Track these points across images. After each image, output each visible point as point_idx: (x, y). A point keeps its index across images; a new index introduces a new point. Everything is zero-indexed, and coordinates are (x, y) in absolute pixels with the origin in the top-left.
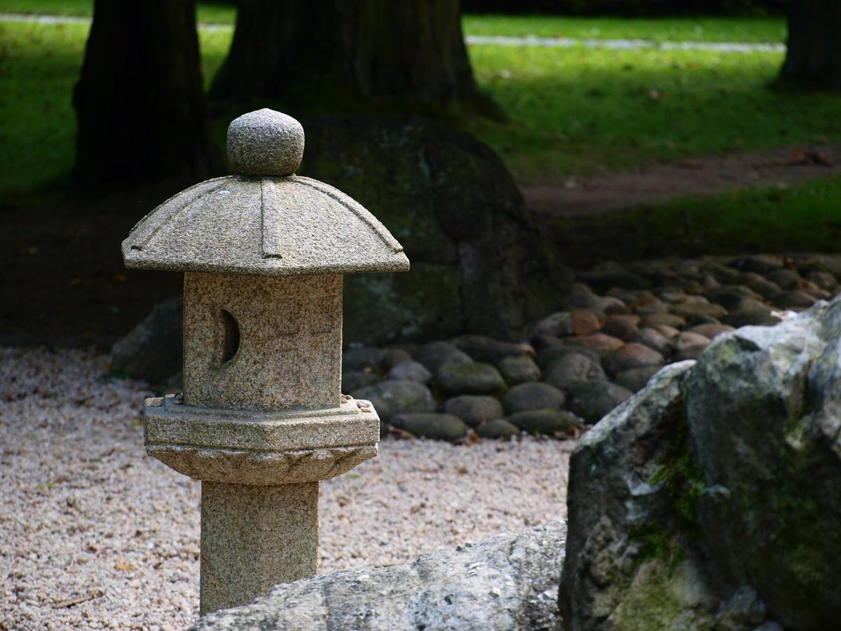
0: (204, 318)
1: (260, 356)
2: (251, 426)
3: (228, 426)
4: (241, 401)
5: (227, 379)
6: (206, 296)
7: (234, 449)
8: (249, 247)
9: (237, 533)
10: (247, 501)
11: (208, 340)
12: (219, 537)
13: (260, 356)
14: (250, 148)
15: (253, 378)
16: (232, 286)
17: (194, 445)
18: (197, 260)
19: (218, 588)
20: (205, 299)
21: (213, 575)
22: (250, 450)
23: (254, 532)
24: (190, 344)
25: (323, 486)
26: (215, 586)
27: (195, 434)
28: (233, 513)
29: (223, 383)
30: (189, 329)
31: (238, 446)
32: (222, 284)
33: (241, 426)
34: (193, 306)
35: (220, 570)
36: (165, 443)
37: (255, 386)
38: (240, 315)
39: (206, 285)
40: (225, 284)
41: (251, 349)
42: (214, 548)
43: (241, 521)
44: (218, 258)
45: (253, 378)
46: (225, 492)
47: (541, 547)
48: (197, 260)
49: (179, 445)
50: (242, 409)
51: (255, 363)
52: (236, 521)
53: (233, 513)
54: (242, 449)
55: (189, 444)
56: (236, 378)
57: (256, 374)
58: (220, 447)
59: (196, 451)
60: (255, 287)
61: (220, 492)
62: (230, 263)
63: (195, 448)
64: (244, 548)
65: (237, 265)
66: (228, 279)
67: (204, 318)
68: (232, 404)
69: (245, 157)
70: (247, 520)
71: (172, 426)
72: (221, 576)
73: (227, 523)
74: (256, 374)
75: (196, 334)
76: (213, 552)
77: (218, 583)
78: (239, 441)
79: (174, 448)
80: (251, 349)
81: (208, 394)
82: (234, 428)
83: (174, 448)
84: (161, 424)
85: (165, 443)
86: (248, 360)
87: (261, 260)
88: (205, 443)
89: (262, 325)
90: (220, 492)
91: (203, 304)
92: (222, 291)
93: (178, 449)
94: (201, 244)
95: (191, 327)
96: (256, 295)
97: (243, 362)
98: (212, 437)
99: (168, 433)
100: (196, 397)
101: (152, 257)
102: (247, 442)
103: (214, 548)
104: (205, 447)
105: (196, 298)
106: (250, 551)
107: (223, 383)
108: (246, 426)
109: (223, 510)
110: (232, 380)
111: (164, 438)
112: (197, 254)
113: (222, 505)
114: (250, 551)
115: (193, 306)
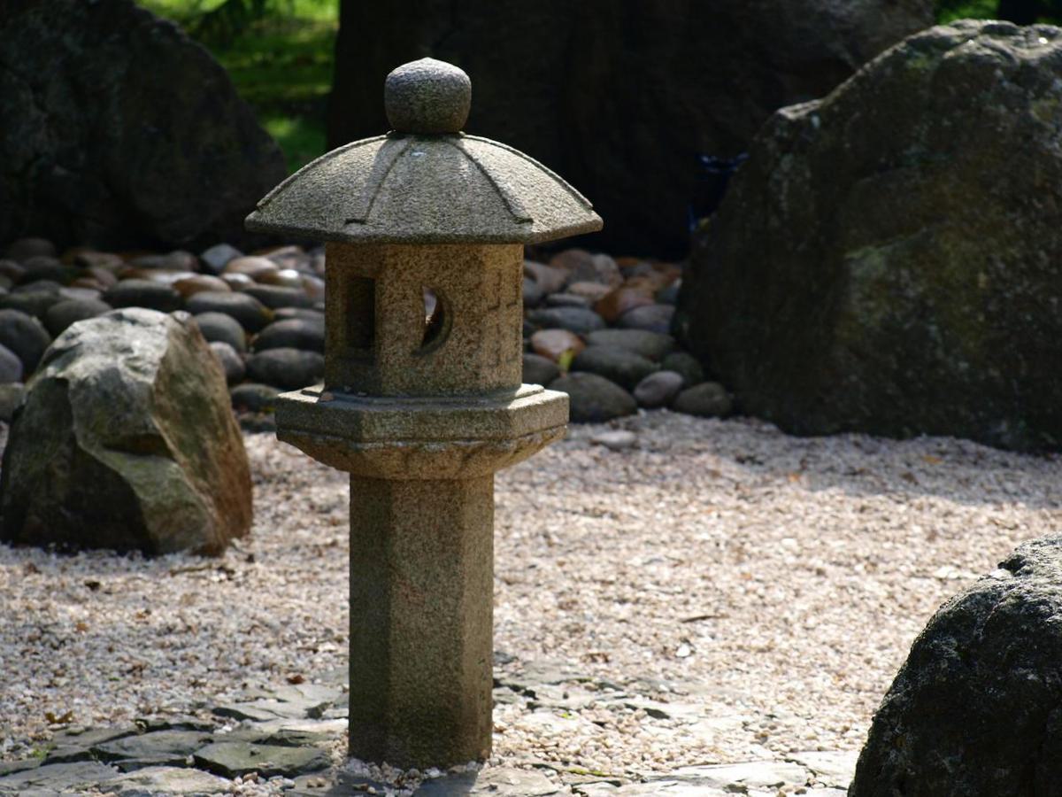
0: (405, 297)
1: (476, 335)
2: (492, 412)
3: (463, 413)
4: (452, 387)
5: (434, 363)
6: (408, 271)
7: (470, 439)
8: (494, 213)
9: (434, 535)
10: (446, 498)
11: (410, 321)
12: (410, 542)
13: (476, 335)
14: (434, 104)
15: (466, 360)
16: (439, 258)
17: (421, 438)
18: (439, 230)
19: (410, 598)
20: (406, 275)
21: (405, 584)
22: (490, 439)
23: (454, 532)
24: (387, 327)
25: (496, 478)
26: (407, 596)
27: (422, 426)
28: (428, 513)
29: (429, 368)
30: (386, 310)
31: (476, 435)
32: (427, 257)
33: (480, 412)
34: (391, 284)
35: (413, 578)
36: (383, 439)
37: (470, 369)
38: (449, 290)
39: (407, 259)
40: (431, 256)
41: (464, 327)
42: (405, 554)
43: (438, 520)
44: (463, 227)
45: (466, 360)
46: (419, 490)
47: (300, 551)
48: (439, 230)
49: (399, 440)
50: (453, 396)
51: (469, 342)
52: (432, 521)
53: (428, 513)
54: (480, 439)
55: (414, 438)
56: (446, 361)
57: (470, 356)
58: (454, 438)
59: (421, 446)
60: (468, 258)
61: (412, 491)
62: (481, 231)
63: (421, 442)
64: (443, 551)
65: (490, 233)
66: (435, 251)
67: (405, 297)
68: (440, 391)
69: (428, 113)
70: (447, 519)
71: (393, 420)
72: (415, 585)
73: (421, 524)
74: (470, 356)
75: (395, 315)
76: (404, 559)
77: (410, 593)
78: (476, 429)
79: (394, 443)
80: (464, 327)
81: (411, 381)
82: (471, 416)
83: (394, 443)
84: (380, 420)
85: (383, 439)
86: (460, 340)
87: (517, 226)
88: (435, 435)
89: (477, 299)
90: (412, 491)
91: (403, 281)
92: (428, 265)
93: (400, 444)
94: (436, 213)
95: (389, 308)
96: (469, 267)
97: (454, 343)
98: (443, 428)
99: (388, 428)
100: (396, 386)
101: (382, 230)
102: (487, 429)
103: (405, 554)
104: (433, 440)
105: (394, 274)
106: (450, 553)
107: (429, 368)
108: (485, 412)
109: (417, 510)
110: (440, 364)
111: (383, 434)
112: (436, 224)
113: (415, 505)
114: (450, 553)
115: (391, 284)
